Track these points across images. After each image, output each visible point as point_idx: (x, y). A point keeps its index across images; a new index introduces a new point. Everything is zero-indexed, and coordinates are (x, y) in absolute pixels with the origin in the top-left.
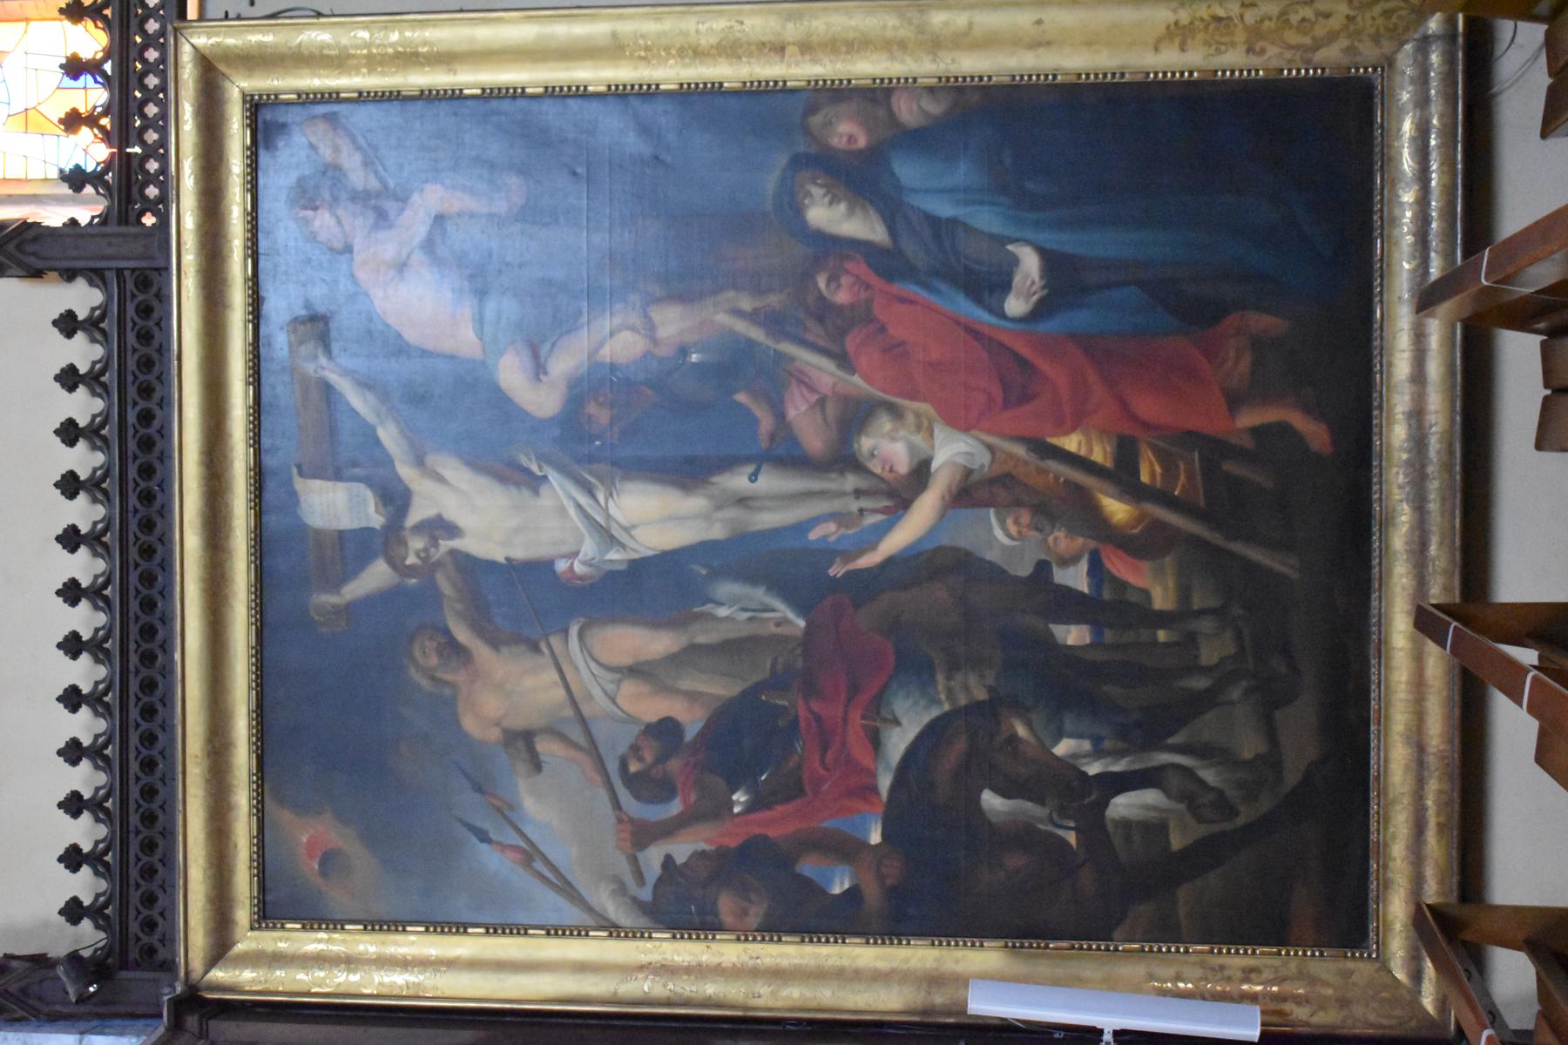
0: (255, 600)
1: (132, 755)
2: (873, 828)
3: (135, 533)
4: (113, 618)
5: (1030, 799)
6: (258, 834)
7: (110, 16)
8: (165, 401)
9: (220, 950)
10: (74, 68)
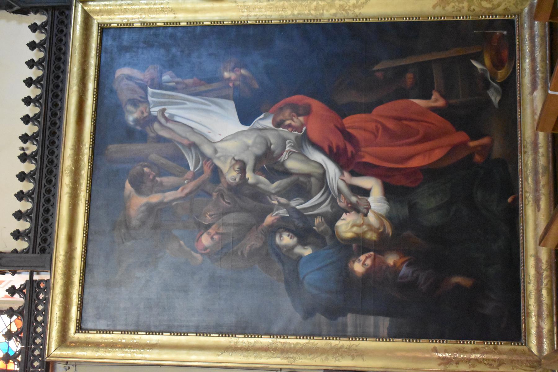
0: (87, 207)
3: (53, 80)
7: (42, 102)
8: (53, 224)
9: (64, 341)
10: (9, 335)
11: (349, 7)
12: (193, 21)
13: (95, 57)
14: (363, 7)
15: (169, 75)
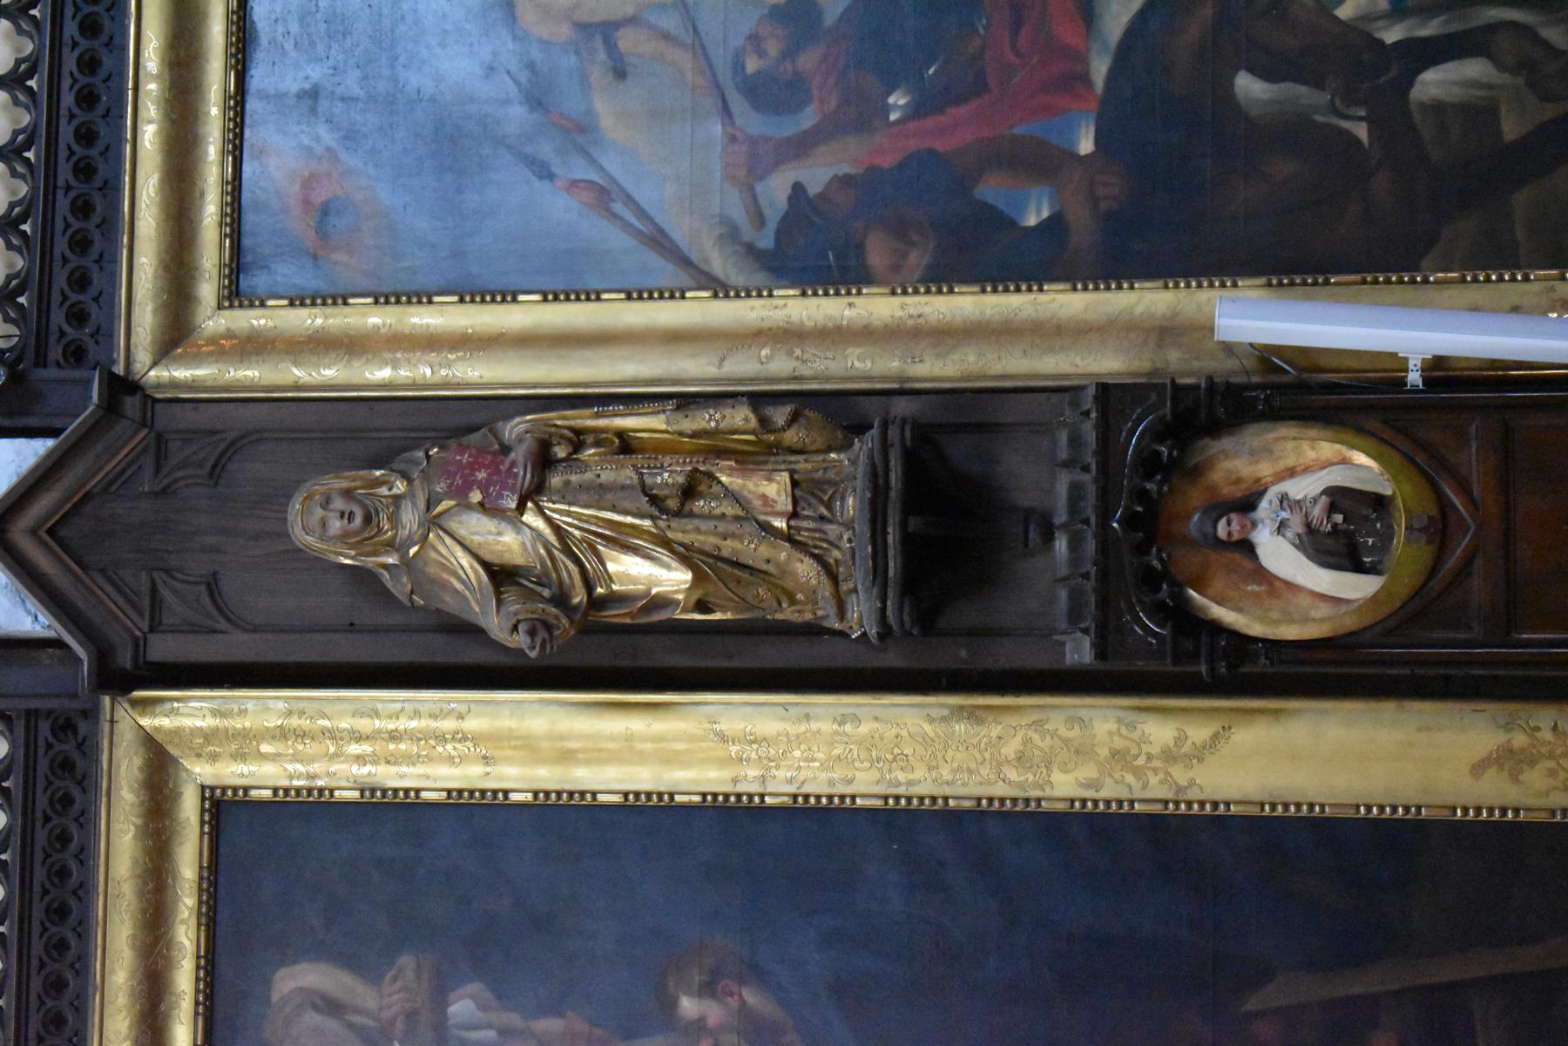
1: (66, 83)
2: (1083, 130)
3: (69, 148)
4: (32, 261)
5: (1305, 82)
6: (237, 93)
7: (35, 88)
8: (106, 256)
11: (1149, 758)
12: (558, 787)
13: (193, 921)
14: (1201, 760)
15: (473, 997)
